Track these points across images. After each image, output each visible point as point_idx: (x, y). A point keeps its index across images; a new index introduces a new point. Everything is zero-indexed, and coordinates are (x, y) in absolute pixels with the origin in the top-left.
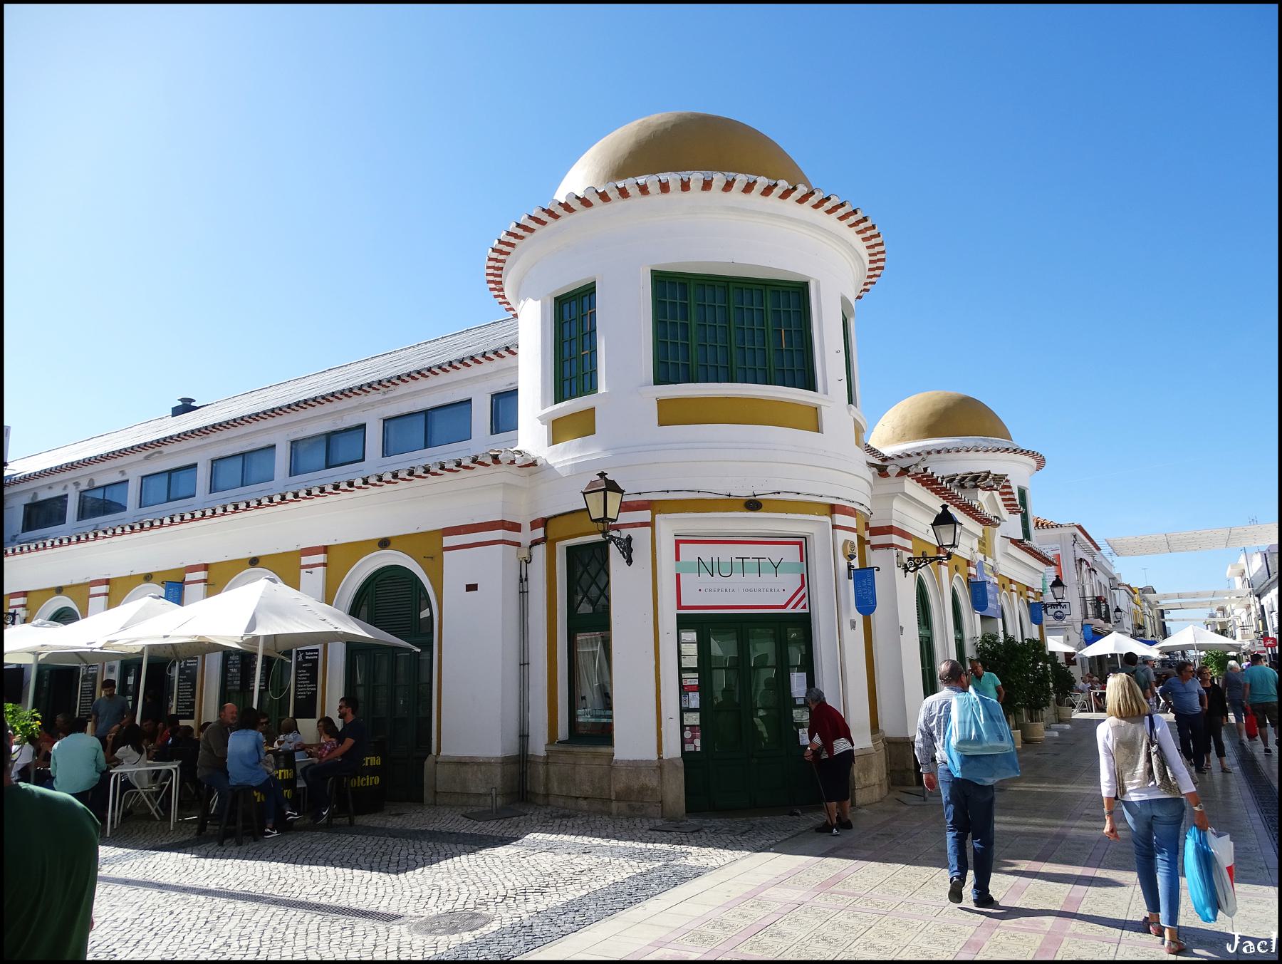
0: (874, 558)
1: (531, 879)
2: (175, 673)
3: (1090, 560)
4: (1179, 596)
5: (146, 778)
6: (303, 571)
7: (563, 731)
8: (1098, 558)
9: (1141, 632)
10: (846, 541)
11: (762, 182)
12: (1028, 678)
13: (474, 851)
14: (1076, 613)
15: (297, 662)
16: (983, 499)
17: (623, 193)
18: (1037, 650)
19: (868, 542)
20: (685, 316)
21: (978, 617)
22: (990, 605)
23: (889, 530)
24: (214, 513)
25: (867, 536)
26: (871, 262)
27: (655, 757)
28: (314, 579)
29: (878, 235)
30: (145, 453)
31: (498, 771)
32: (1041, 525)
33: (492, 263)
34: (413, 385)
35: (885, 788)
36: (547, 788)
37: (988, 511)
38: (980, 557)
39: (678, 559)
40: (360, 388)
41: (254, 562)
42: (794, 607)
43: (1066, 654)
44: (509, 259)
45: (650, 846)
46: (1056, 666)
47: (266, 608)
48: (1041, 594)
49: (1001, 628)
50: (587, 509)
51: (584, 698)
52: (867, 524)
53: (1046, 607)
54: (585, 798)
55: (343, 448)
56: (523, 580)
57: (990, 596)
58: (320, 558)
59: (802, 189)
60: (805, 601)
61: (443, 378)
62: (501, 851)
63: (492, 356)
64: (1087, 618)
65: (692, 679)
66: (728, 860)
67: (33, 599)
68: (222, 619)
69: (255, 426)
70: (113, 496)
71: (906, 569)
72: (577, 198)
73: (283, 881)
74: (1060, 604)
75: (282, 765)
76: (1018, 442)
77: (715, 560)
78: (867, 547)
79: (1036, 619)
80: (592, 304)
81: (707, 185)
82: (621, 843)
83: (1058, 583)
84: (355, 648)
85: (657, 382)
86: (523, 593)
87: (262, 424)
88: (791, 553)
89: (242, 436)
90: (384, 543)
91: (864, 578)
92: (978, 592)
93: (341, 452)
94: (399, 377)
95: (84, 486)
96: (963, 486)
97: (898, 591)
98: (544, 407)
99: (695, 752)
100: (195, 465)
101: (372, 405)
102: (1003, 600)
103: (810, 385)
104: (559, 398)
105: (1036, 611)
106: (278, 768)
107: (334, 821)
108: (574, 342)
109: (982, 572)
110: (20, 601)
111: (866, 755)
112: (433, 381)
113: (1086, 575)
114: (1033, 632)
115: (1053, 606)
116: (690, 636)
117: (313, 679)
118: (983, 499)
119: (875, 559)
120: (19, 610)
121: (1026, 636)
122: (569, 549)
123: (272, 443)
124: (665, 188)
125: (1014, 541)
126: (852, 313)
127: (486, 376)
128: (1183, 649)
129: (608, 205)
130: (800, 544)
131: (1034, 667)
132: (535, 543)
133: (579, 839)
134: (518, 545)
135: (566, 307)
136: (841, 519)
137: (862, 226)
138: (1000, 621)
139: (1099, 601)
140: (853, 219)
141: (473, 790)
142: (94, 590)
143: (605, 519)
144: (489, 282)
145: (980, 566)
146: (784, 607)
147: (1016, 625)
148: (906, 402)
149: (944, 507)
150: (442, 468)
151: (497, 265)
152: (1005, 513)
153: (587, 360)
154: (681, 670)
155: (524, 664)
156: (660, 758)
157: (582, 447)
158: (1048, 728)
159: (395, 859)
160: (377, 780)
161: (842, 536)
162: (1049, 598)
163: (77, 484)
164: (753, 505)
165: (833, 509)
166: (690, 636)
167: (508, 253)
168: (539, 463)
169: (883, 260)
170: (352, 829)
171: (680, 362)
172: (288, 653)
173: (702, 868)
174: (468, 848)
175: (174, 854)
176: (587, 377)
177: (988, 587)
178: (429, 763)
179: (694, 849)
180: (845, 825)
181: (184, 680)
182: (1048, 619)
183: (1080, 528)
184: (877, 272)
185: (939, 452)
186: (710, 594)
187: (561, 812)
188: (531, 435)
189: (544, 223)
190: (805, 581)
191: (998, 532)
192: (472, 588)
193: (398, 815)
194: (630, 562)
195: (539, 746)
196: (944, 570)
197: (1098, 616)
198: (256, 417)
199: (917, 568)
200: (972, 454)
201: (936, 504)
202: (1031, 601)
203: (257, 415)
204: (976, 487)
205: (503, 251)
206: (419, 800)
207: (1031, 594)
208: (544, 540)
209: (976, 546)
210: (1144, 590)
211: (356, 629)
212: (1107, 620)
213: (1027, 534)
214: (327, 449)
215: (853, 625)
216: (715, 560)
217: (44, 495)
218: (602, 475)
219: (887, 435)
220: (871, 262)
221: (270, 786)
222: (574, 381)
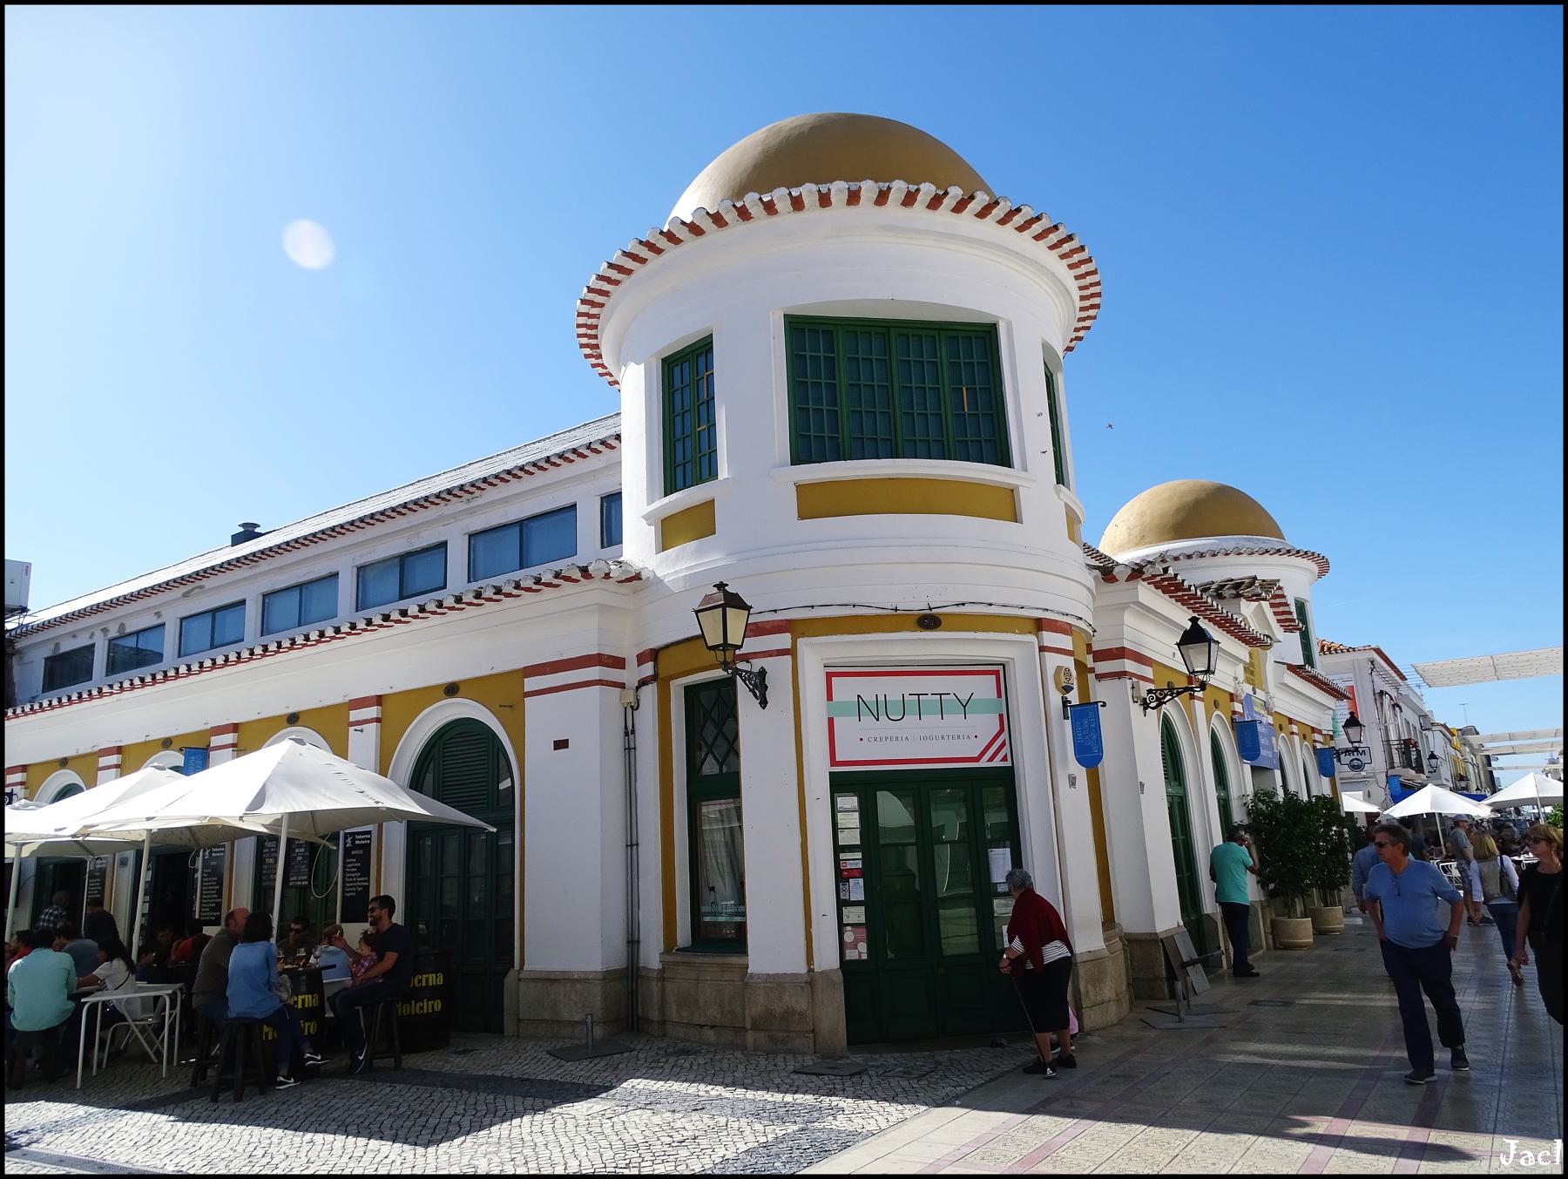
0: (1099, 691)
1: (608, 1154)
2: (199, 864)
3: (1394, 693)
4: (1511, 737)
5: (138, 1006)
6: (351, 729)
7: (683, 936)
8: (1403, 691)
9: (1463, 784)
10: (1059, 669)
11: (927, 190)
12: (1318, 847)
13: (544, 1109)
14: (1378, 762)
15: (345, 848)
16: (1247, 611)
17: (744, 214)
18: (1329, 810)
19: (1092, 670)
20: (832, 373)
21: (1247, 768)
22: (1263, 752)
23: (1120, 653)
24: (239, 657)
25: (1089, 661)
26: (1082, 298)
27: (803, 970)
28: (364, 740)
29: (1089, 260)
30: (184, 589)
31: (597, 990)
32: (1327, 650)
33: (583, 320)
34: (503, 490)
35: (1126, 1005)
36: (662, 1009)
37: (1255, 627)
38: (1248, 689)
39: (830, 697)
40: (438, 496)
41: (293, 719)
42: (991, 759)
43: (1368, 815)
44: (603, 312)
45: (789, 1098)
46: (1354, 830)
47: (287, 776)
48: (1332, 738)
49: (1279, 782)
50: (703, 636)
51: (712, 889)
52: (1089, 646)
53: (1338, 753)
54: (713, 1027)
55: (421, 574)
56: (629, 732)
57: (1263, 741)
58: (373, 712)
59: (981, 199)
60: (1006, 750)
61: (540, 478)
62: (582, 1108)
63: (600, 448)
64: (1392, 767)
65: (854, 860)
66: (893, 1119)
67: (35, 773)
68: (225, 795)
69: (312, 550)
70: (146, 643)
71: (1145, 705)
72: (683, 223)
73: (268, 1159)
74: (1356, 749)
75: (303, 989)
76: (1292, 541)
77: (881, 698)
78: (1091, 677)
79: (1326, 770)
80: (709, 366)
81: (853, 198)
82: (750, 1094)
83: (1353, 722)
84: (416, 829)
85: (796, 460)
86: (630, 750)
87: (322, 547)
88: (983, 687)
89: (298, 563)
90: (452, 690)
91: (1084, 717)
92: (1247, 735)
93: (419, 578)
94: (485, 480)
95: (113, 633)
96: (1219, 596)
97: (1135, 735)
98: (650, 501)
99: (859, 962)
100: (243, 602)
101: (454, 517)
102: (1281, 746)
103: (1004, 459)
104: (670, 488)
105: (1326, 759)
106: (296, 993)
107: (376, 1063)
108: (687, 416)
109: (1251, 710)
110: (18, 777)
111: (1095, 959)
112: (527, 483)
113: (1388, 712)
114: (1323, 787)
115: (1347, 751)
116: (849, 802)
117: (365, 870)
118: (1247, 611)
119: (1101, 691)
120: (17, 789)
121: (1314, 792)
122: (689, 690)
123: (334, 570)
124: (797, 204)
125: (1292, 668)
126: (1059, 367)
127: (594, 473)
128: (1517, 806)
129: (725, 232)
130: (996, 673)
131: (1326, 833)
132: (643, 683)
133: (693, 1088)
134: (622, 686)
135: (677, 370)
136: (1050, 638)
137: (1066, 247)
138: (1278, 773)
139: (1407, 745)
140: (1053, 238)
141: (566, 1016)
142: (103, 761)
143: (725, 646)
144: (582, 346)
145: (1248, 701)
146: (977, 759)
147: (1300, 778)
148: (1144, 495)
149: (1194, 620)
150: (517, 586)
151: (590, 322)
152: (1278, 631)
153: (705, 436)
154: (838, 849)
155: (632, 845)
156: (811, 971)
157: (699, 552)
158: (1347, 913)
159: (433, 1122)
160: (438, 1005)
161: (1054, 661)
162: (1342, 742)
163: (105, 631)
164: (929, 621)
165: (1039, 625)
166: (849, 802)
167: (602, 305)
168: (644, 576)
169: (1098, 295)
170: (398, 1076)
171: (826, 434)
172: (334, 838)
173: (855, 1134)
174: (538, 1102)
175: (148, 1115)
176: (705, 461)
177: (1260, 728)
178: (510, 980)
179: (847, 1103)
180: (1066, 1062)
181: (210, 875)
182: (1342, 770)
183: (1378, 651)
184: (1092, 312)
185: (1189, 557)
186: (868, 744)
187: (680, 1045)
188: (638, 544)
189: (643, 261)
190: (1005, 723)
191: (1271, 656)
192: (561, 744)
193: (465, 1052)
194: (764, 703)
195: (652, 955)
196: (1199, 707)
197: (1407, 763)
198: (313, 538)
199: (1160, 703)
200: (1233, 558)
201: (1182, 617)
202: (1319, 746)
203: (314, 535)
204: (1238, 596)
205: (596, 300)
206: (500, 1030)
207: (1317, 737)
208: (654, 678)
209: (1241, 675)
210: (1463, 732)
211: (410, 805)
212: (1419, 769)
213: (1309, 659)
214: (400, 574)
215: (1073, 781)
216: (881, 698)
217: (67, 646)
218: (721, 586)
219: (1121, 541)
220: (1082, 298)
221: (284, 1018)
222: (688, 467)
